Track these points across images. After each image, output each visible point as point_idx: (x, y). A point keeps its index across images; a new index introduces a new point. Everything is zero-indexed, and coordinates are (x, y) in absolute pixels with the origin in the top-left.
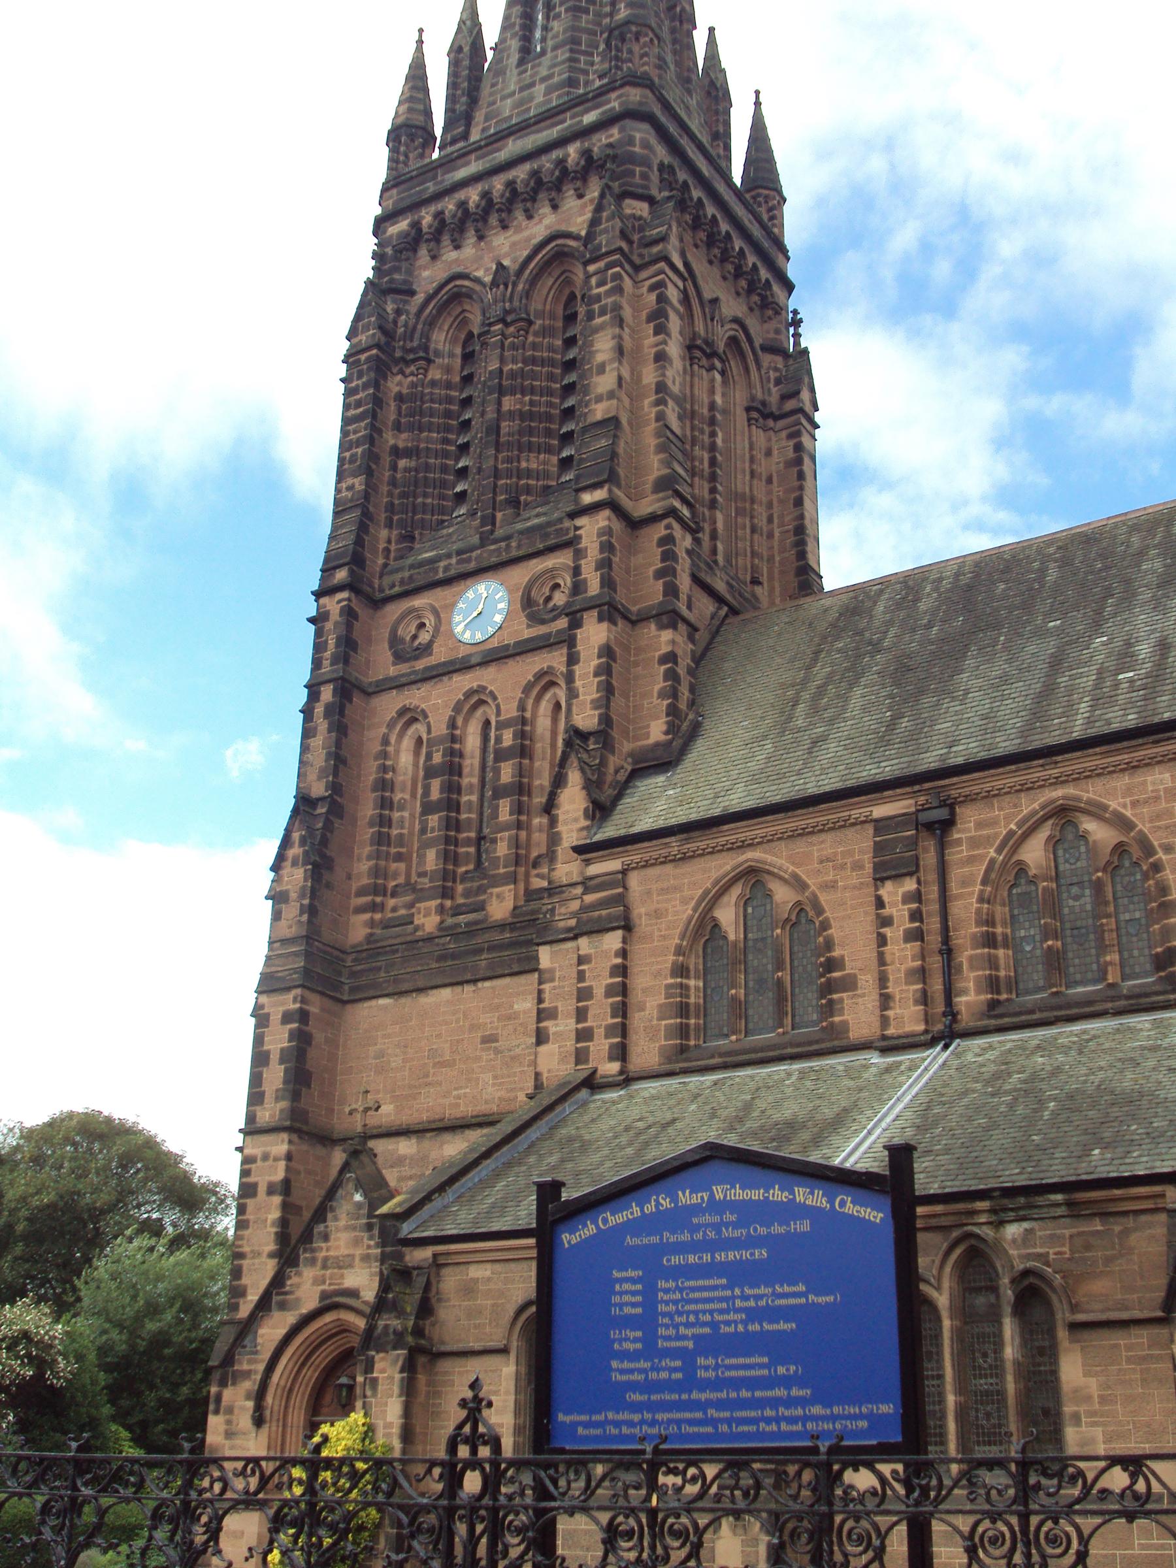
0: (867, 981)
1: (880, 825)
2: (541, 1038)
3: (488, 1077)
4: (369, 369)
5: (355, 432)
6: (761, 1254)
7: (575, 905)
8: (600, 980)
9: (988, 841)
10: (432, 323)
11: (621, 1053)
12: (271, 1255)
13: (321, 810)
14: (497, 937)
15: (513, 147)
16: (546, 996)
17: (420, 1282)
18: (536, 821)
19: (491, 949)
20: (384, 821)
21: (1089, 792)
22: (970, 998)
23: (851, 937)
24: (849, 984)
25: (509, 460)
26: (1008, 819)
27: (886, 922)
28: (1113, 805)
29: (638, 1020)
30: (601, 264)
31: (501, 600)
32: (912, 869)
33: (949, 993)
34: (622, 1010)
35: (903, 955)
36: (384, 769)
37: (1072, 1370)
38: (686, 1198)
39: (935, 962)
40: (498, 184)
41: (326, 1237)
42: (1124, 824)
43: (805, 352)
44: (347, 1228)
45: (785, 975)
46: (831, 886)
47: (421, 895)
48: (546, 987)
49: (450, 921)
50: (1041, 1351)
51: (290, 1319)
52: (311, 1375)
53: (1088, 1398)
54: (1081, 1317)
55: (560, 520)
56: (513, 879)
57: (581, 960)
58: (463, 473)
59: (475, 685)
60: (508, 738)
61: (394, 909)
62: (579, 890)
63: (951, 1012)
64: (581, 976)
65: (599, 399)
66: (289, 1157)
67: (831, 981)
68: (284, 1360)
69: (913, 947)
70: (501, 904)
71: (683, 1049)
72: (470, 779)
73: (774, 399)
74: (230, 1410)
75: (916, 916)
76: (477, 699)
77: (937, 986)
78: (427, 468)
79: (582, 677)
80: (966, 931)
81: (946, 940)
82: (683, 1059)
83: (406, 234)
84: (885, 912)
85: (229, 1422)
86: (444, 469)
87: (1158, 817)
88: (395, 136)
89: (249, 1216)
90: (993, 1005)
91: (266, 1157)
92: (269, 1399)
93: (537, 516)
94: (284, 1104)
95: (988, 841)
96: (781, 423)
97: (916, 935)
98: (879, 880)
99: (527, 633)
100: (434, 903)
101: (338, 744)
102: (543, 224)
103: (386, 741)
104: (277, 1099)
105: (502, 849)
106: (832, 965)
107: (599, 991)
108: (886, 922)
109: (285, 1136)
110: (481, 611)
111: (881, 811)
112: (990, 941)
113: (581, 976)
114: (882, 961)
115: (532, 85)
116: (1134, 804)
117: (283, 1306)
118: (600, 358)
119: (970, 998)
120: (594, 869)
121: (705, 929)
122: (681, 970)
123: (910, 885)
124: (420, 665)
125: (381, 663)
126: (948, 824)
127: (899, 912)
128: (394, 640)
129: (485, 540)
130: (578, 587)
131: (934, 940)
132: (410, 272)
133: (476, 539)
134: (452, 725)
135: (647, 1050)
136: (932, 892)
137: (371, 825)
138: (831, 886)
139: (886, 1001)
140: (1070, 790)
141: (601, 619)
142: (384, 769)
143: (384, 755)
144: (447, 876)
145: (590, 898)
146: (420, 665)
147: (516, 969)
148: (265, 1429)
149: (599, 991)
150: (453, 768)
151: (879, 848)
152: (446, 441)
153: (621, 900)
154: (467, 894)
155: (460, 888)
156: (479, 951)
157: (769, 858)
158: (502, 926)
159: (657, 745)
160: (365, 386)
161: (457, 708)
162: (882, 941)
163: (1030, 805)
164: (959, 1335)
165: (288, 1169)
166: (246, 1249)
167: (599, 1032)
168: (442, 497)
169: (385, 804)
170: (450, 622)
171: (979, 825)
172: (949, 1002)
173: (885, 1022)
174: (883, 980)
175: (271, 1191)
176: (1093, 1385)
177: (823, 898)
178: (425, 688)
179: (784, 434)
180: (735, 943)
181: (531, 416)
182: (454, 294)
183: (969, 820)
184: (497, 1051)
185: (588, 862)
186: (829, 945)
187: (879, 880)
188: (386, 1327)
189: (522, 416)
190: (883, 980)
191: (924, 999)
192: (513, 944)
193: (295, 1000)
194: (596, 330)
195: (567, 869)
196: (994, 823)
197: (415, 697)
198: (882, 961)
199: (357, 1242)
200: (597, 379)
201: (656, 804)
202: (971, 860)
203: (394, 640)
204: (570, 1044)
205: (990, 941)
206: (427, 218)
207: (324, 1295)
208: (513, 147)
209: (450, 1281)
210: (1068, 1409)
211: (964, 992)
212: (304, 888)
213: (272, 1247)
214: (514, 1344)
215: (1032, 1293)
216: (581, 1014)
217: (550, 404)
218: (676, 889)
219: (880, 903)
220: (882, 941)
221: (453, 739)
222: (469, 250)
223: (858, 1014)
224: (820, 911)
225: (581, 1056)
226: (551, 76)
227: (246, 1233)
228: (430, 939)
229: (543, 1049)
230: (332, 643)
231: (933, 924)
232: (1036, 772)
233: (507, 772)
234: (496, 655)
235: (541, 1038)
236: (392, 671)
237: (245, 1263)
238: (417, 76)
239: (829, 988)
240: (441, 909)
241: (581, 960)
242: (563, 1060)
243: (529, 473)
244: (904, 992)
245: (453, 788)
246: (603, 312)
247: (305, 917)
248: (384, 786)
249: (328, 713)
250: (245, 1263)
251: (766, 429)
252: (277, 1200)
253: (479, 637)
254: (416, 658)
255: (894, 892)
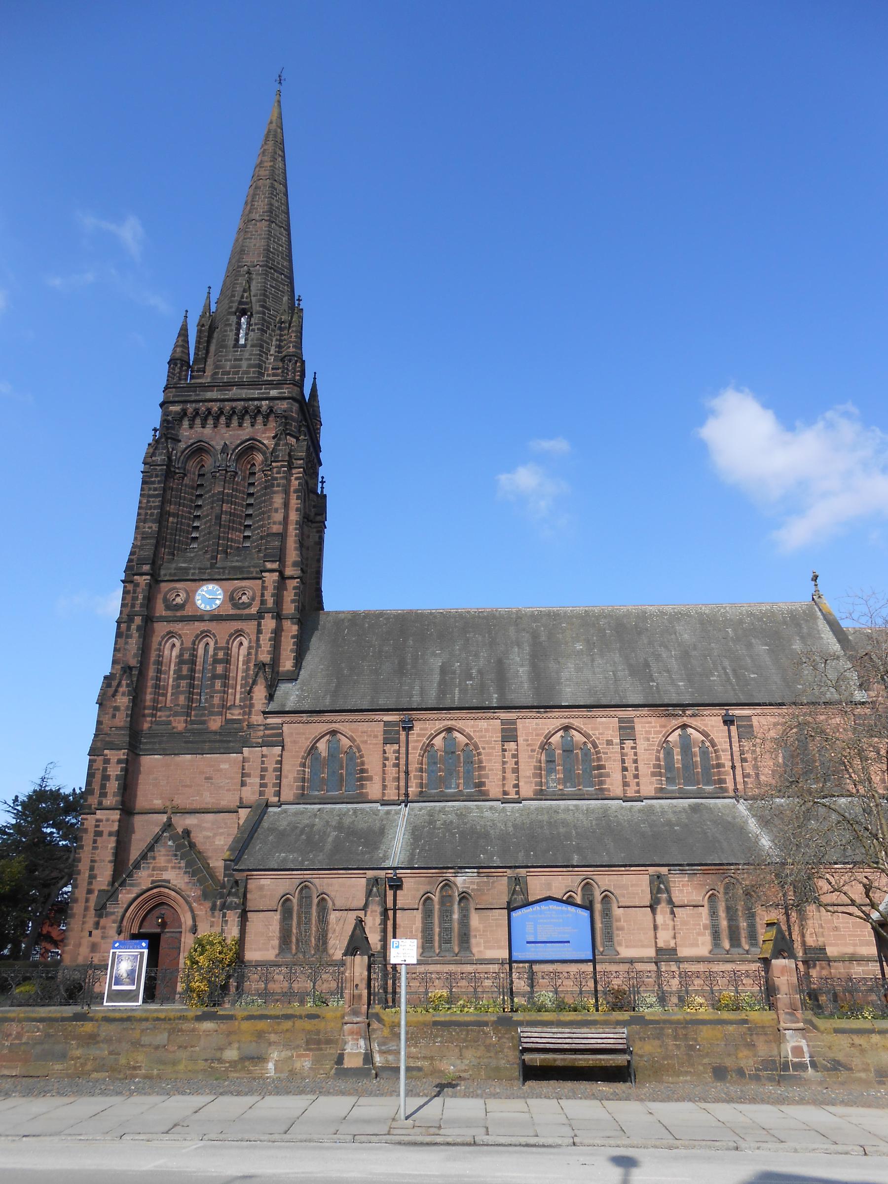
0: (377, 779)
1: (386, 724)
2: (243, 784)
3: (208, 794)
4: (162, 475)
5: (153, 502)
6: (561, 920)
7: (261, 733)
8: (271, 765)
9: (424, 735)
10: (188, 458)
11: (278, 794)
12: (110, 862)
13: (135, 672)
14: (213, 737)
15: (234, 392)
16: (246, 767)
17: (242, 885)
18: (230, 691)
19: (210, 741)
20: (158, 679)
21: (459, 724)
22: (413, 790)
23: (372, 762)
24: (370, 779)
25: (224, 533)
26: (431, 729)
27: (387, 759)
28: (467, 730)
29: (284, 782)
30: (279, 464)
31: (220, 594)
32: (398, 742)
33: (407, 787)
34: (279, 777)
35: (391, 771)
36: (159, 656)
37: (475, 920)
38: (543, 907)
39: (402, 775)
40: (228, 406)
41: (154, 858)
42: (468, 737)
43: (325, 496)
44: (164, 855)
45: (344, 772)
46: (365, 742)
47: (176, 714)
48: (246, 764)
49: (189, 727)
50: (464, 916)
51: (136, 890)
52: (142, 913)
53: (479, 931)
54: (479, 907)
55: (249, 567)
56: (220, 714)
57: (263, 756)
58: (196, 528)
59: (206, 629)
60: (221, 655)
61: (160, 717)
62: (262, 728)
63: (407, 795)
64: (263, 762)
65: (274, 523)
66: (120, 821)
67: (362, 776)
68: (132, 907)
69: (395, 769)
70: (215, 723)
71: (303, 794)
72: (199, 667)
73: (312, 514)
74: (104, 928)
75: (397, 758)
76: (205, 634)
77: (402, 783)
78: (182, 523)
79: (263, 640)
80: (413, 767)
81: (407, 767)
82: (302, 798)
83: (176, 413)
84: (387, 755)
85: (103, 933)
86: (189, 525)
87: (482, 737)
88: (172, 362)
89: (99, 844)
90: (421, 792)
91: (108, 820)
92: (125, 923)
93: (237, 561)
94: (118, 798)
95: (424, 735)
96: (315, 525)
97: (397, 765)
98: (385, 744)
99: (232, 612)
100: (182, 718)
101: (143, 644)
102: (247, 432)
103: (160, 644)
104: (114, 796)
105: (216, 700)
106: (363, 771)
107: (270, 769)
108: (387, 759)
109: (118, 812)
110: (209, 596)
111: (386, 718)
112: (421, 770)
113: (263, 762)
114: (384, 773)
115: (241, 360)
116: (474, 731)
117: (132, 885)
118: (276, 505)
119: (413, 790)
120: (269, 721)
121: (312, 749)
122: (303, 765)
123: (396, 747)
124: (179, 614)
125: (160, 610)
126: (411, 728)
127: (391, 756)
128: (165, 600)
129: (213, 566)
130: (263, 602)
131: (403, 768)
132: (178, 431)
133: (208, 564)
134: (194, 643)
135: (288, 794)
136: (403, 750)
137: (152, 679)
138: (365, 742)
139: (384, 787)
140: (453, 722)
141: (273, 618)
142: (159, 656)
143: (159, 650)
144: (189, 708)
145: (267, 732)
146: (179, 614)
147: (222, 751)
148: (122, 935)
149: (270, 769)
150: (193, 662)
151: (385, 732)
152: (190, 513)
153: (281, 735)
154: (196, 716)
155: (193, 713)
156: (205, 742)
157: (342, 728)
158: (215, 733)
159: (288, 671)
160: (159, 482)
161: (197, 636)
162: (385, 765)
163: (440, 725)
164: (440, 910)
165: (119, 826)
166: (97, 858)
167: (270, 785)
168: (187, 538)
169: (159, 671)
170: (194, 598)
171: (421, 729)
172: (407, 790)
173: (384, 794)
174: (384, 780)
175: (110, 834)
176: (481, 927)
177: (362, 746)
178: (180, 625)
179: (315, 530)
180: (325, 757)
181: (234, 515)
182: (199, 450)
183: (418, 727)
184: (212, 784)
185: (266, 718)
186: (363, 763)
187: (385, 744)
188: (232, 902)
189: (231, 514)
190: (384, 780)
191: (398, 788)
192: (221, 741)
193: (124, 754)
194: (275, 492)
195: (257, 719)
196: (426, 729)
197: (177, 627)
198: (384, 773)
199: (169, 861)
200: (274, 514)
201: (290, 694)
202: (417, 741)
203: (165, 600)
204: (257, 788)
205: (421, 770)
206: (190, 408)
207: (153, 882)
208: (234, 392)
209: (252, 885)
210: (472, 933)
211: (412, 787)
212: (128, 706)
213: (111, 858)
214: (279, 908)
215: (464, 897)
216: (262, 777)
217: (242, 511)
218: (304, 734)
219: (385, 752)
220: (385, 765)
221: (194, 649)
222: (208, 431)
223: (373, 789)
224: (359, 750)
225: (261, 793)
226: (250, 359)
227: (97, 852)
228: (180, 733)
229: (243, 788)
230: (141, 597)
231: (403, 762)
232: (444, 714)
233: (220, 669)
234: (216, 618)
235: (243, 784)
236: (164, 613)
237: (96, 865)
238: (183, 333)
239: (361, 779)
240: (186, 721)
241: (263, 756)
242: (253, 793)
243: (232, 540)
244: (391, 785)
245: (193, 670)
246: (278, 486)
247: (129, 719)
248: (159, 663)
249: (139, 629)
250: (96, 865)
251: (307, 526)
252: (114, 839)
253: (208, 608)
254: (177, 610)
255: (388, 747)
